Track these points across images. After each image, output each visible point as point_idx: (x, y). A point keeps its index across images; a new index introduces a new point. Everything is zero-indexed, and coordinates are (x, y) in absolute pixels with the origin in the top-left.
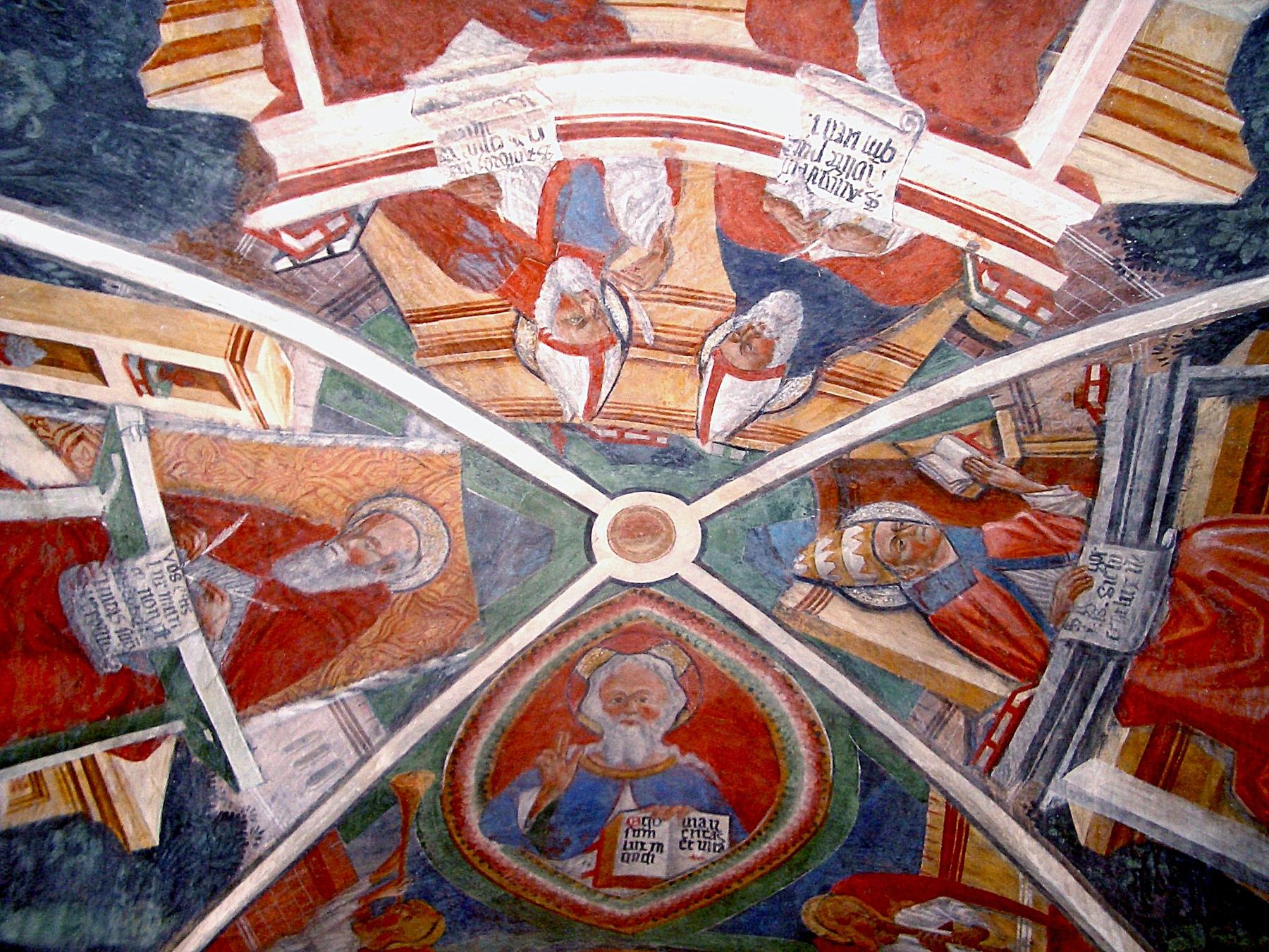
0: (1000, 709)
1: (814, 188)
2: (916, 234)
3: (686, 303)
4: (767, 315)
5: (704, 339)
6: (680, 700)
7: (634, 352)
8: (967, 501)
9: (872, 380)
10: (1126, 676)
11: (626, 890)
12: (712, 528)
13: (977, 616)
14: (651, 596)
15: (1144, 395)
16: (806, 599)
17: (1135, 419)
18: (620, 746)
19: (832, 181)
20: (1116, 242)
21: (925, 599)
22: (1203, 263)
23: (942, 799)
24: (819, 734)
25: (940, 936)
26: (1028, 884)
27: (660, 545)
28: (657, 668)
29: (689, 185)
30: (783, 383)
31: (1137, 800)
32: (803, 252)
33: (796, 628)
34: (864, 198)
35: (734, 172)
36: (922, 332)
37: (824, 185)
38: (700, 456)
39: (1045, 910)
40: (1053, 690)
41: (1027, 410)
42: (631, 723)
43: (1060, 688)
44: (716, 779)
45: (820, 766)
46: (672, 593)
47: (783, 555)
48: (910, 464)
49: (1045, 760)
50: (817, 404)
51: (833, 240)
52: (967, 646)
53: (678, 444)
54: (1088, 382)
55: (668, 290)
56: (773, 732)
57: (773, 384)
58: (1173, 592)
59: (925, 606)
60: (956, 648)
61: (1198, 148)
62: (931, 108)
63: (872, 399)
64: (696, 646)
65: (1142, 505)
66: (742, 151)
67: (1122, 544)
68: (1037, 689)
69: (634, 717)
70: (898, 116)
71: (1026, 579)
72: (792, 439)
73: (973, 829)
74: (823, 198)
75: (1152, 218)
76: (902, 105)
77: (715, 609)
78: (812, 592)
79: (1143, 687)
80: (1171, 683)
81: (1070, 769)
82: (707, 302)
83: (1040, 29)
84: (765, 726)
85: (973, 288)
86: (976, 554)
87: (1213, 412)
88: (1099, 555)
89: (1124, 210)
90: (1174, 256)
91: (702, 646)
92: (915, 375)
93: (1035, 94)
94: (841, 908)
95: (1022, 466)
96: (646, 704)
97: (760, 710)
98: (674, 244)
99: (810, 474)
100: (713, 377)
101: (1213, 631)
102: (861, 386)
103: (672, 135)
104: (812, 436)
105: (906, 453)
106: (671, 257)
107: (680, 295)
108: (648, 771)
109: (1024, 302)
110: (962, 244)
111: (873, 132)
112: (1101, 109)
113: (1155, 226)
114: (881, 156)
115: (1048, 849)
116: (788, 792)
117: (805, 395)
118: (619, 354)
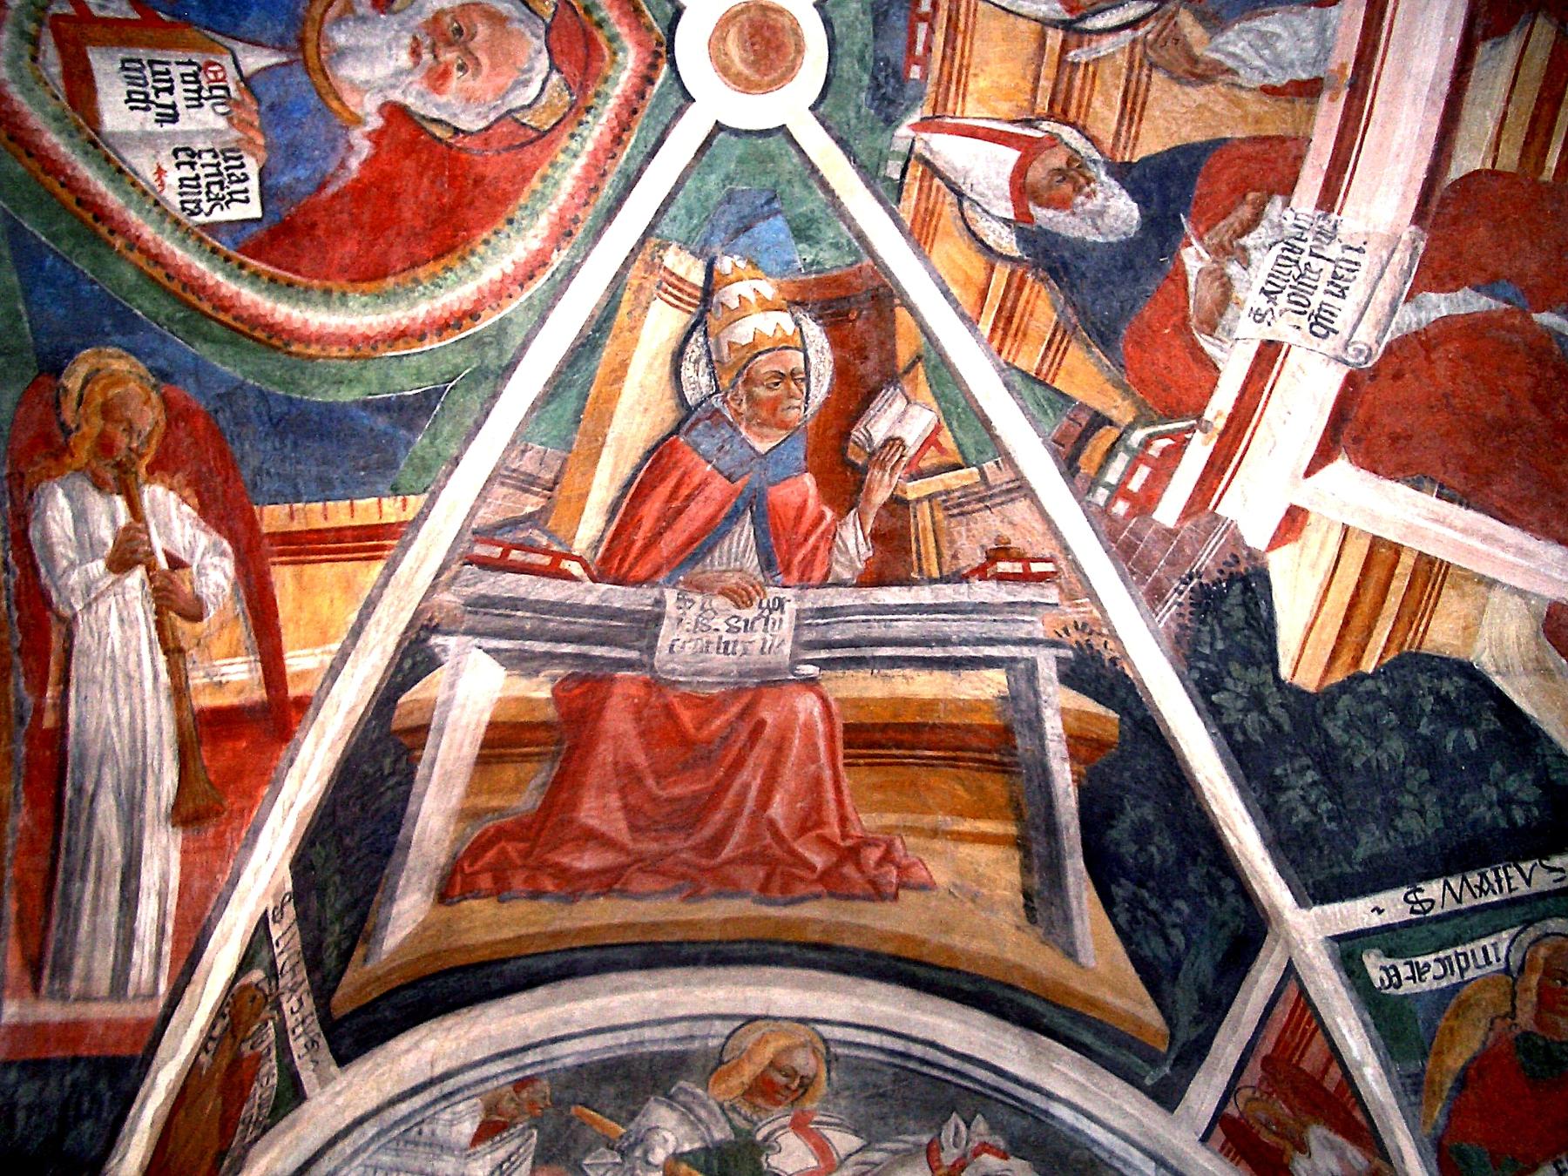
0: (555, 548)
1: (1277, 250)
2: (1220, 366)
3: (1124, 102)
4: (1106, 199)
5: (1073, 125)
6: (470, 122)
7: (1055, 38)
8: (842, 451)
9: (1014, 326)
10: (620, 674)
11: (56, 70)
12: (773, 144)
13: (685, 492)
14: (654, 67)
15: (1010, 617)
16: (680, 279)
17: (971, 612)
18: (365, 41)
19: (1286, 270)
20: (1221, 572)
21: (700, 426)
22: (1206, 658)
23: (410, 515)
24: (459, 327)
25: (152, 553)
26: (328, 659)
27: (739, 74)
28: (526, 83)
29: (1287, 105)
30: (1006, 221)
31: (459, 735)
32: (1193, 240)
33: (632, 272)
34: (1265, 307)
35: (1300, 159)
36: (1085, 377)
37: (1281, 261)
38: (890, 122)
39: (293, 691)
40: (590, 600)
41: (981, 500)
42: (415, 53)
43: (596, 607)
44: (332, 189)
45: (399, 336)
46: (661, 96)
47: (743, 240)
48: (891, 377)
49: (489, 619)
50: (975, 265)
51: (1210, 273)
52: (636, 491)
53: (910, 93)
54: (1020, 558)
55: (1144, 79)
56: (443, 262)
57: (1006, 209)
58: (740, 690)
59: (689, 430)
60: (634, 476)
61: (1340, 637)
62: (1375, 373)
63: (985, 327)
64: (572, 136)
65: (849, 635)
66: (1325, 167)
67: (797, 627)
68: (589, 583)
69: (427, 57)
70: (1364, 339)
71: (744, 534)
72: (919, 235)
73: (378, 567)
74: (1264, 263)
75: (1257, 604)
76: (1378, 343)
77: (640, 158)
78: (694, 286)
79: (609, 695)
80: (618, 720)
81: (487, 651)
82: (1124, 128)
83: (1462, 474)
84: (451, 249)
85: (1151, 430)
86: (770, 474)
87: (992, 684)
88: (781, 606)
89: (1264, 577)
90: (1212, 632)
91: (574, 145)
92: (1025, 374)
93: (1390, 476)
94: (135, 404)
95: (897, 503)
96: (456, 74)
97: (480, 239)
98: (1207, 88)
99: (867, 261)
100: (1017, 136)
101: (686, 742)
102: (1005, 314)
103: (1353, 86)
104: (924, 258)
105: (907, 372)
106: (1189, 83)
107: (1136, 95)
108: (326, 91)
109: (1135, 485)
110: (1208, 415)
111: (1345, 312)
112: (1376, 541)
113: (1247, 609)
114: (1317, 323)
115: (388, 667)
116: (336, 295)
117: (989, 248)
118: (1053, 15)
